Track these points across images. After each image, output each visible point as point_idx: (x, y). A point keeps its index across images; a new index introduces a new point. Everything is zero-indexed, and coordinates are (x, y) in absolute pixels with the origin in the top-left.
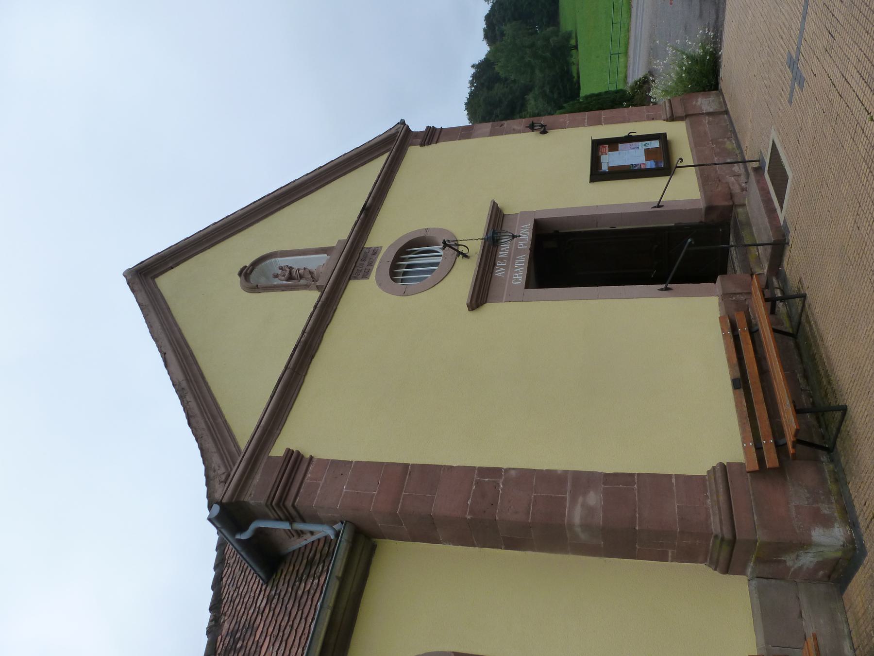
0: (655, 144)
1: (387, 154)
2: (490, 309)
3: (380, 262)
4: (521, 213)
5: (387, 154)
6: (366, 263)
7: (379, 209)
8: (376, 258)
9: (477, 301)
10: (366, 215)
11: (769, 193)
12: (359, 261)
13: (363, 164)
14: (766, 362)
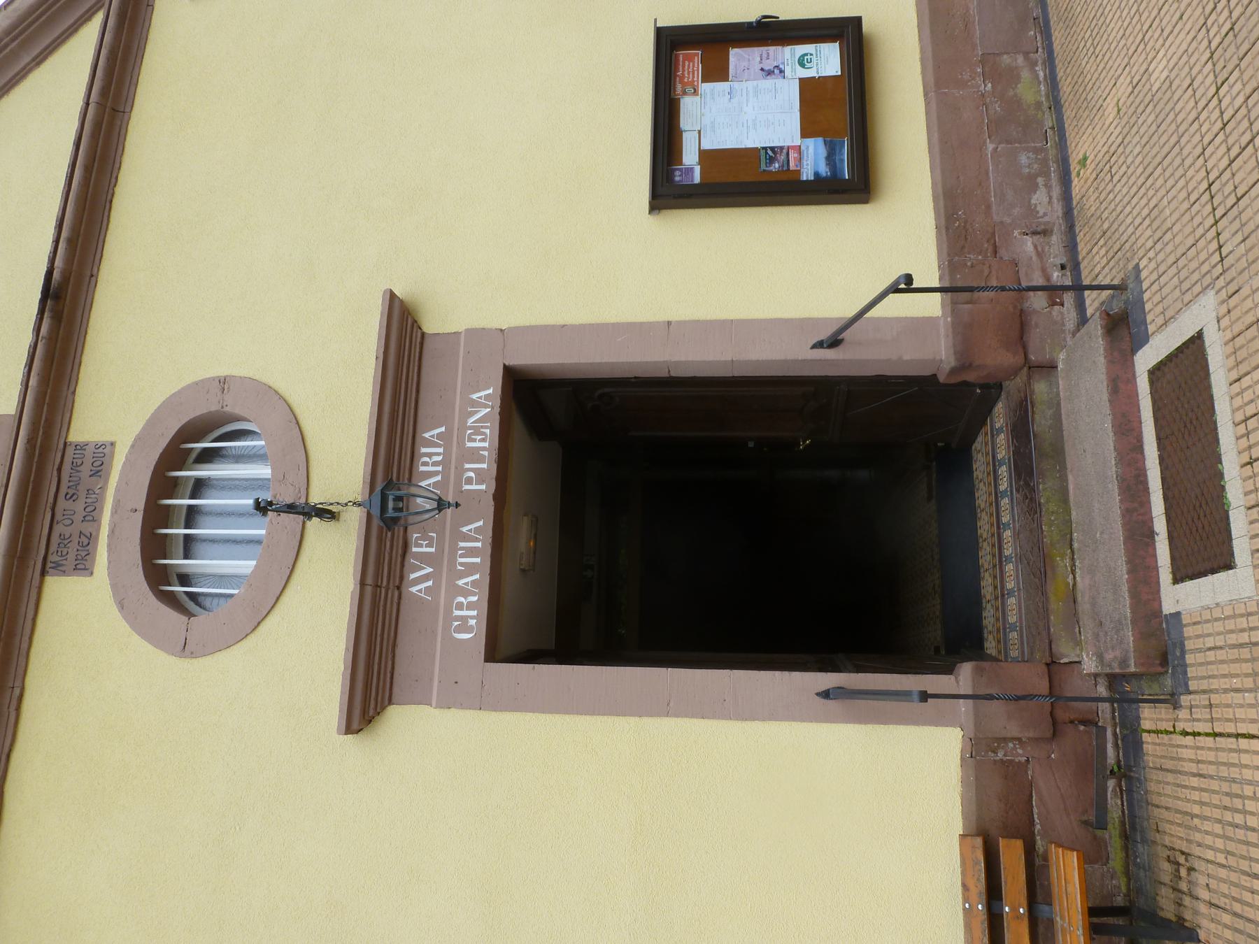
0: (827, 60)
1: (98, 19)
2: (404, 722)
3: (115, 511)
4: (467, 330)
5: (98, 19)
6: (79, 506)
7: (93, 276)
8: (103, 489)
9: (364, 712)
10: (57, 318)
11: (1139, 447)
12: (62, 504)
13: (39, 60)
14: (1048, 879)
